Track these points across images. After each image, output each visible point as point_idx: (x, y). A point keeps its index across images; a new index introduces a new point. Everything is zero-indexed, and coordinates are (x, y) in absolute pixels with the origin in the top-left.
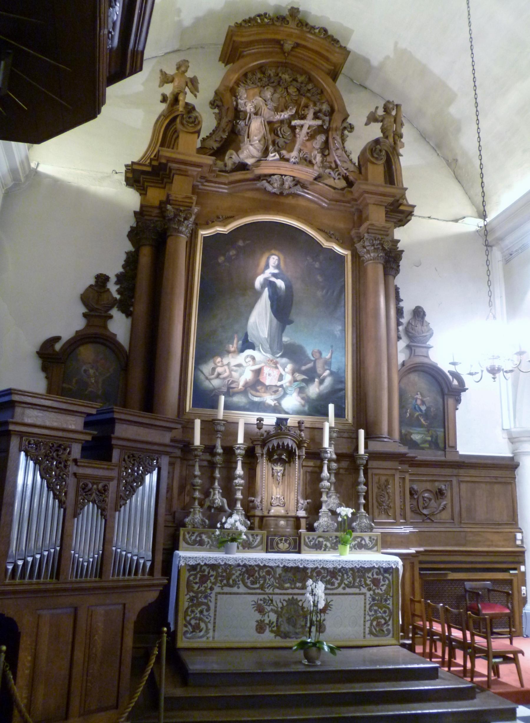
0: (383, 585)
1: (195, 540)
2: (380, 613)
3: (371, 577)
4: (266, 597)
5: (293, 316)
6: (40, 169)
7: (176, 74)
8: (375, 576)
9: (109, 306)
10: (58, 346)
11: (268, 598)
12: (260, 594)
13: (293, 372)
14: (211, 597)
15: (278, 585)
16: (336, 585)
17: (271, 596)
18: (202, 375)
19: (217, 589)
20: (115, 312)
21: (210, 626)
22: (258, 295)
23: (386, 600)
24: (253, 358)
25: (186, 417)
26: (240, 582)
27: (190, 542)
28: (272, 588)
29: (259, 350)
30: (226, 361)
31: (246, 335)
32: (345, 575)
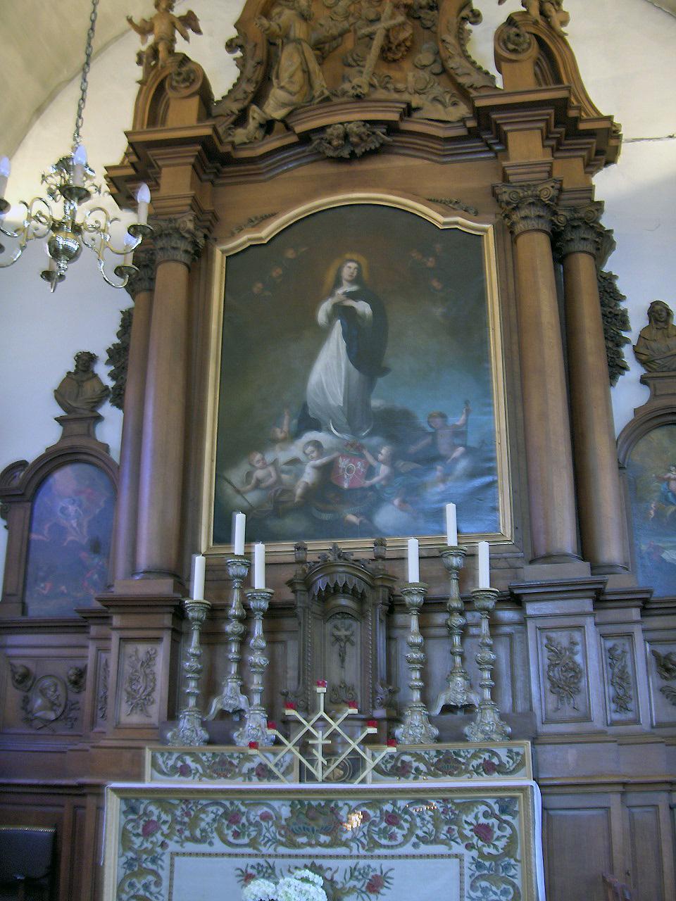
0: (498, 839)
1: (174, 768)
2: (495, 894)
3: (474, 822)
4: (262, 861)
5: (390, 360)
7: (156, 16)
8: (482, 820)
9: (96, 400)
11: (265, 865)
12: (250, 855)
14: (162, 861)
15: (283, 840)
16: (400, 838)
17: (271, 861)
18: (229, 486)
19: (173, 846)
22: (322, 334)
23: (506, 868)
24: (317, 445)
26: (215, 835)
27: (165, 770)
28: (273, 847)
29: (329, 431)
30: (269, 457)
31: (305, 407)
32: (418, 820)
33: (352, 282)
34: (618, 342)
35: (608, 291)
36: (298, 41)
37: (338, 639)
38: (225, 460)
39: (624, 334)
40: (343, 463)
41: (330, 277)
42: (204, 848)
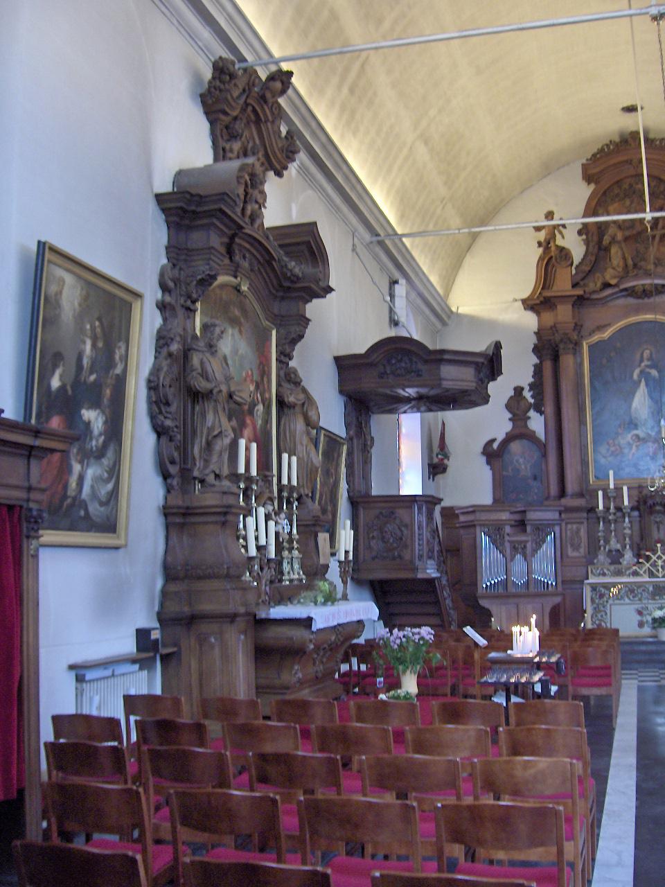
6: (459, 311)
10: (495, 446)
22: (638, 384)
25: (591, 487)
33: (648, 360)
36: (619, 242)
37: (657, 522)
42: (622, 602)
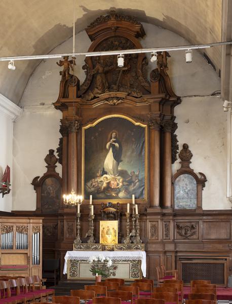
5: (122, 158)
13: (123, 182)
20: (57, 164)
21: (78, 273)
22: (108, 151)
24: (107, 178)
30: (96, 180)
31: (104, 169)
33: (114, 138)
34: (176, 153)
35: (174, 139)
38: (86, 181)
39: (177, 151)
40: (112, 182)
41: (109, 137)
